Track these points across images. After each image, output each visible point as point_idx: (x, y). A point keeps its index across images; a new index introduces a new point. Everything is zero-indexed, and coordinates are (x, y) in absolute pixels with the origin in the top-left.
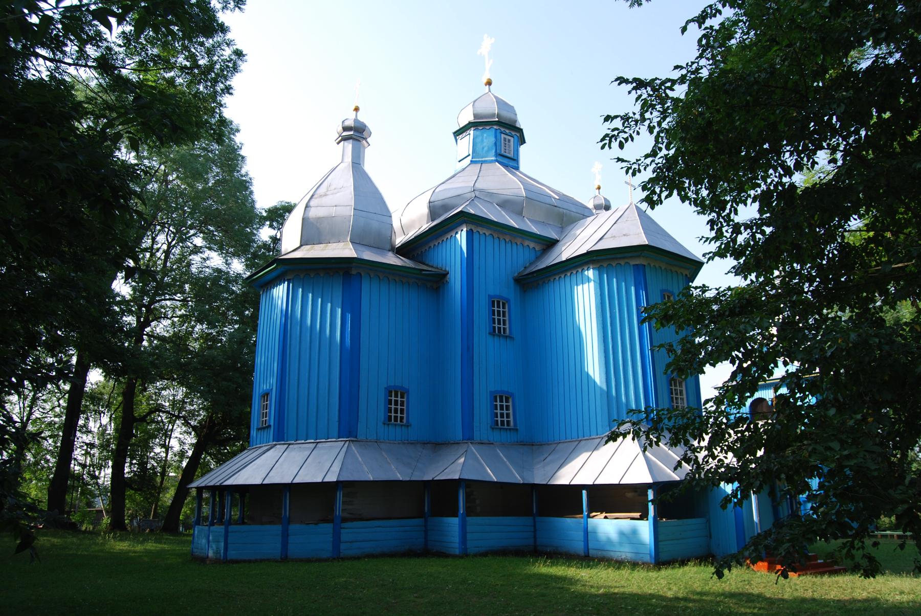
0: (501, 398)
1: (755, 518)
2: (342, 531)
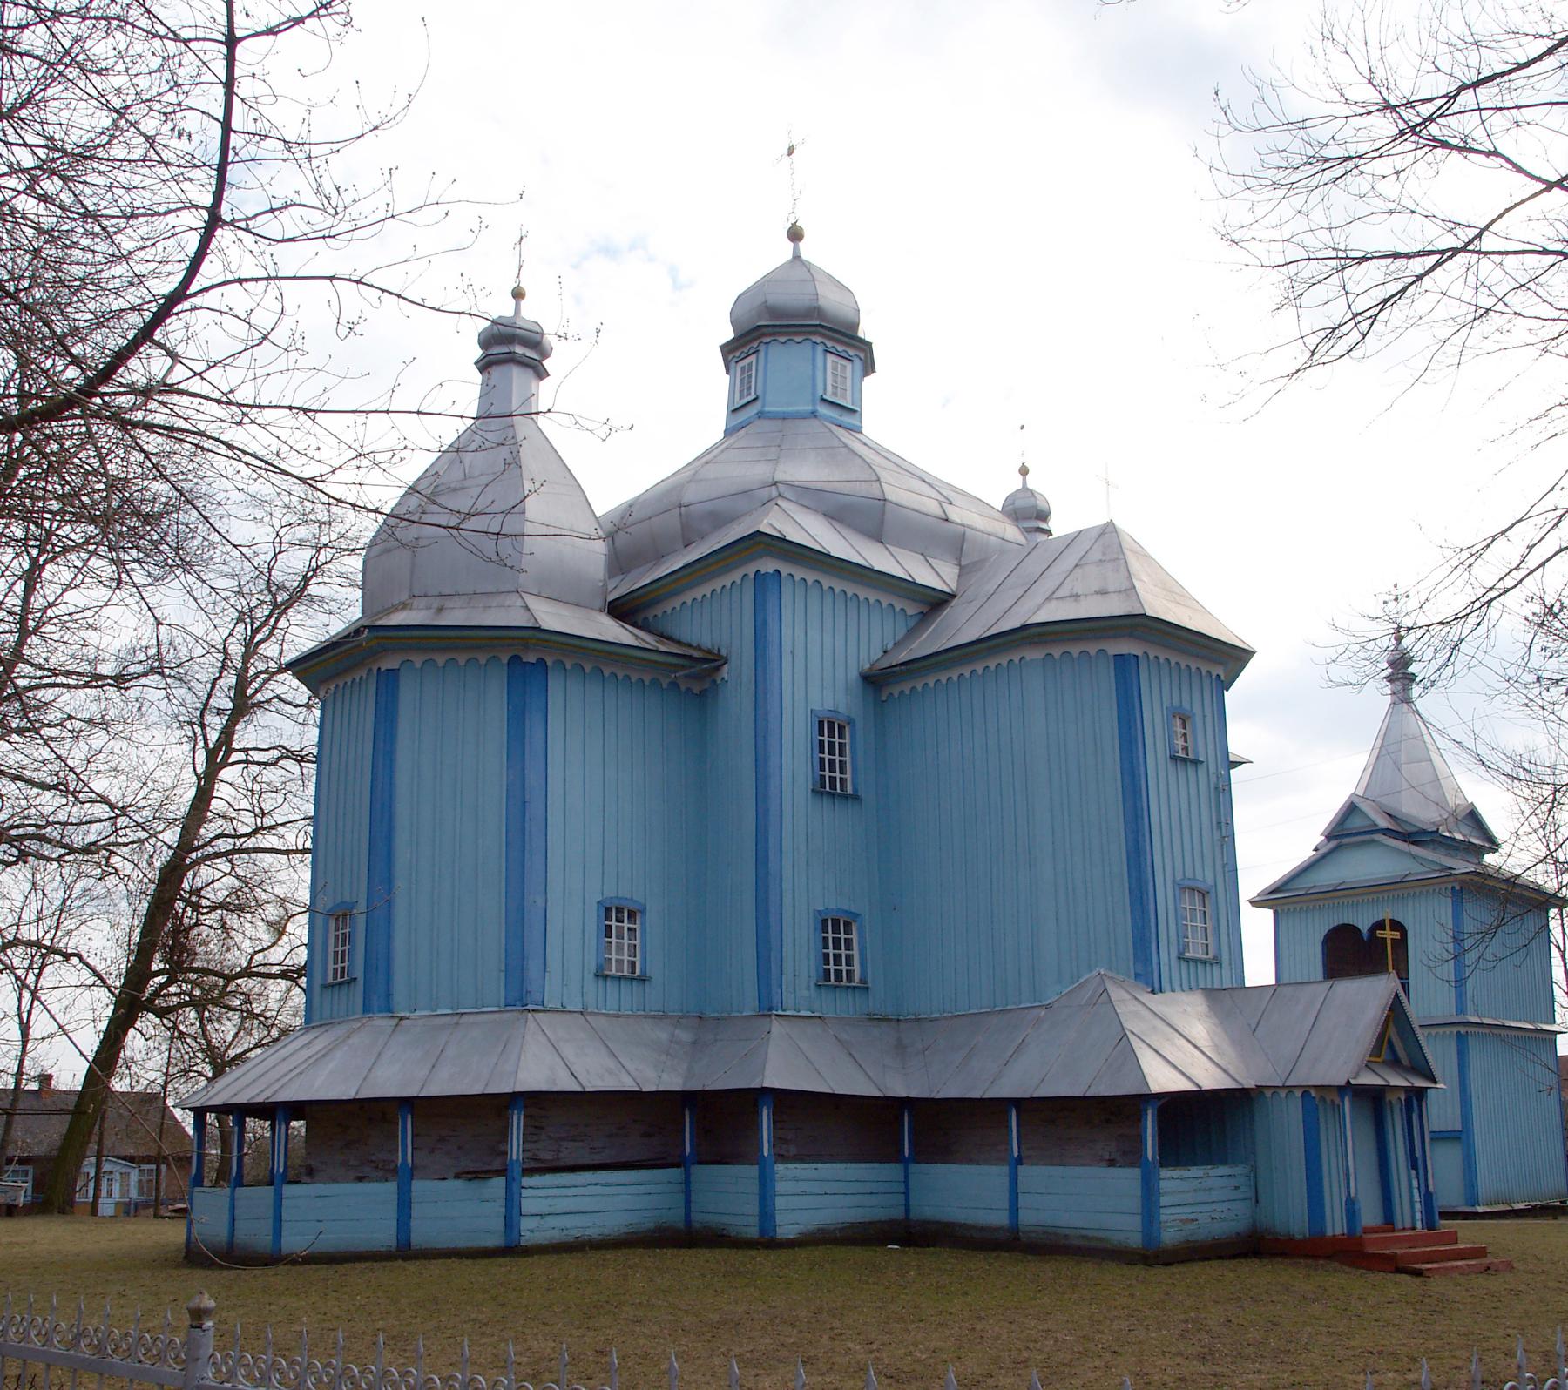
0: (834, 925)
1: (688, 1150)
2: (525, 1193)
